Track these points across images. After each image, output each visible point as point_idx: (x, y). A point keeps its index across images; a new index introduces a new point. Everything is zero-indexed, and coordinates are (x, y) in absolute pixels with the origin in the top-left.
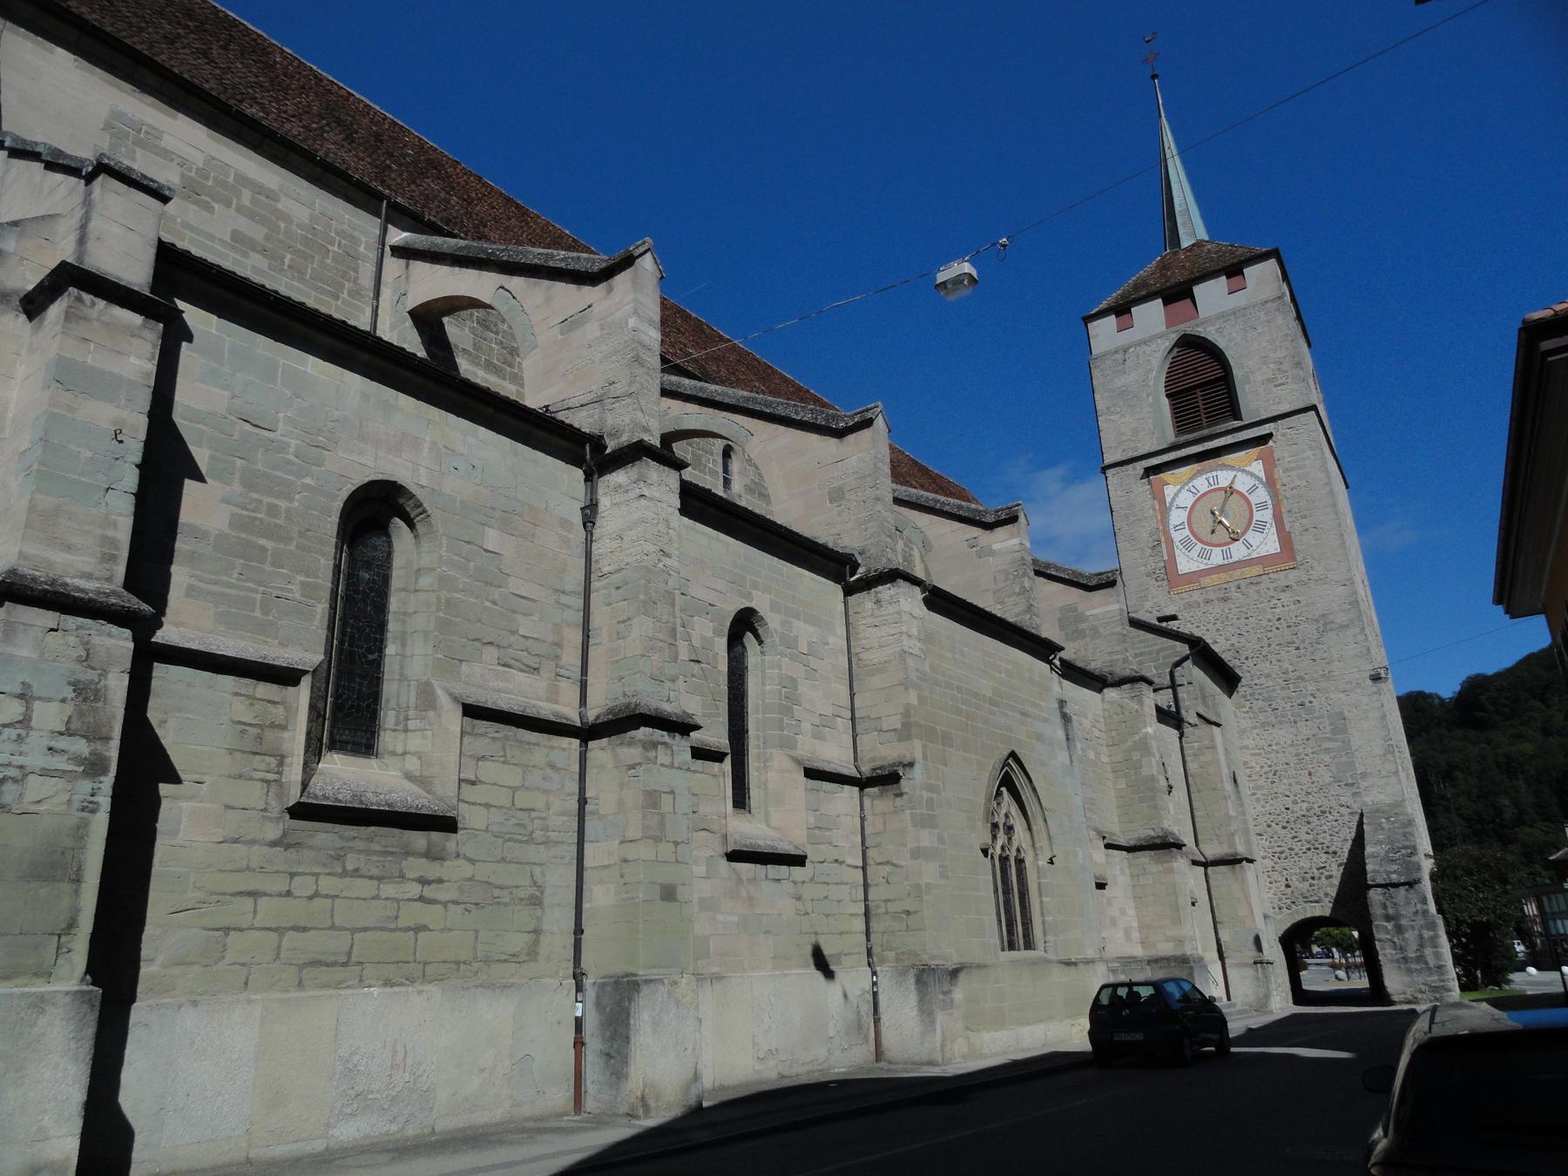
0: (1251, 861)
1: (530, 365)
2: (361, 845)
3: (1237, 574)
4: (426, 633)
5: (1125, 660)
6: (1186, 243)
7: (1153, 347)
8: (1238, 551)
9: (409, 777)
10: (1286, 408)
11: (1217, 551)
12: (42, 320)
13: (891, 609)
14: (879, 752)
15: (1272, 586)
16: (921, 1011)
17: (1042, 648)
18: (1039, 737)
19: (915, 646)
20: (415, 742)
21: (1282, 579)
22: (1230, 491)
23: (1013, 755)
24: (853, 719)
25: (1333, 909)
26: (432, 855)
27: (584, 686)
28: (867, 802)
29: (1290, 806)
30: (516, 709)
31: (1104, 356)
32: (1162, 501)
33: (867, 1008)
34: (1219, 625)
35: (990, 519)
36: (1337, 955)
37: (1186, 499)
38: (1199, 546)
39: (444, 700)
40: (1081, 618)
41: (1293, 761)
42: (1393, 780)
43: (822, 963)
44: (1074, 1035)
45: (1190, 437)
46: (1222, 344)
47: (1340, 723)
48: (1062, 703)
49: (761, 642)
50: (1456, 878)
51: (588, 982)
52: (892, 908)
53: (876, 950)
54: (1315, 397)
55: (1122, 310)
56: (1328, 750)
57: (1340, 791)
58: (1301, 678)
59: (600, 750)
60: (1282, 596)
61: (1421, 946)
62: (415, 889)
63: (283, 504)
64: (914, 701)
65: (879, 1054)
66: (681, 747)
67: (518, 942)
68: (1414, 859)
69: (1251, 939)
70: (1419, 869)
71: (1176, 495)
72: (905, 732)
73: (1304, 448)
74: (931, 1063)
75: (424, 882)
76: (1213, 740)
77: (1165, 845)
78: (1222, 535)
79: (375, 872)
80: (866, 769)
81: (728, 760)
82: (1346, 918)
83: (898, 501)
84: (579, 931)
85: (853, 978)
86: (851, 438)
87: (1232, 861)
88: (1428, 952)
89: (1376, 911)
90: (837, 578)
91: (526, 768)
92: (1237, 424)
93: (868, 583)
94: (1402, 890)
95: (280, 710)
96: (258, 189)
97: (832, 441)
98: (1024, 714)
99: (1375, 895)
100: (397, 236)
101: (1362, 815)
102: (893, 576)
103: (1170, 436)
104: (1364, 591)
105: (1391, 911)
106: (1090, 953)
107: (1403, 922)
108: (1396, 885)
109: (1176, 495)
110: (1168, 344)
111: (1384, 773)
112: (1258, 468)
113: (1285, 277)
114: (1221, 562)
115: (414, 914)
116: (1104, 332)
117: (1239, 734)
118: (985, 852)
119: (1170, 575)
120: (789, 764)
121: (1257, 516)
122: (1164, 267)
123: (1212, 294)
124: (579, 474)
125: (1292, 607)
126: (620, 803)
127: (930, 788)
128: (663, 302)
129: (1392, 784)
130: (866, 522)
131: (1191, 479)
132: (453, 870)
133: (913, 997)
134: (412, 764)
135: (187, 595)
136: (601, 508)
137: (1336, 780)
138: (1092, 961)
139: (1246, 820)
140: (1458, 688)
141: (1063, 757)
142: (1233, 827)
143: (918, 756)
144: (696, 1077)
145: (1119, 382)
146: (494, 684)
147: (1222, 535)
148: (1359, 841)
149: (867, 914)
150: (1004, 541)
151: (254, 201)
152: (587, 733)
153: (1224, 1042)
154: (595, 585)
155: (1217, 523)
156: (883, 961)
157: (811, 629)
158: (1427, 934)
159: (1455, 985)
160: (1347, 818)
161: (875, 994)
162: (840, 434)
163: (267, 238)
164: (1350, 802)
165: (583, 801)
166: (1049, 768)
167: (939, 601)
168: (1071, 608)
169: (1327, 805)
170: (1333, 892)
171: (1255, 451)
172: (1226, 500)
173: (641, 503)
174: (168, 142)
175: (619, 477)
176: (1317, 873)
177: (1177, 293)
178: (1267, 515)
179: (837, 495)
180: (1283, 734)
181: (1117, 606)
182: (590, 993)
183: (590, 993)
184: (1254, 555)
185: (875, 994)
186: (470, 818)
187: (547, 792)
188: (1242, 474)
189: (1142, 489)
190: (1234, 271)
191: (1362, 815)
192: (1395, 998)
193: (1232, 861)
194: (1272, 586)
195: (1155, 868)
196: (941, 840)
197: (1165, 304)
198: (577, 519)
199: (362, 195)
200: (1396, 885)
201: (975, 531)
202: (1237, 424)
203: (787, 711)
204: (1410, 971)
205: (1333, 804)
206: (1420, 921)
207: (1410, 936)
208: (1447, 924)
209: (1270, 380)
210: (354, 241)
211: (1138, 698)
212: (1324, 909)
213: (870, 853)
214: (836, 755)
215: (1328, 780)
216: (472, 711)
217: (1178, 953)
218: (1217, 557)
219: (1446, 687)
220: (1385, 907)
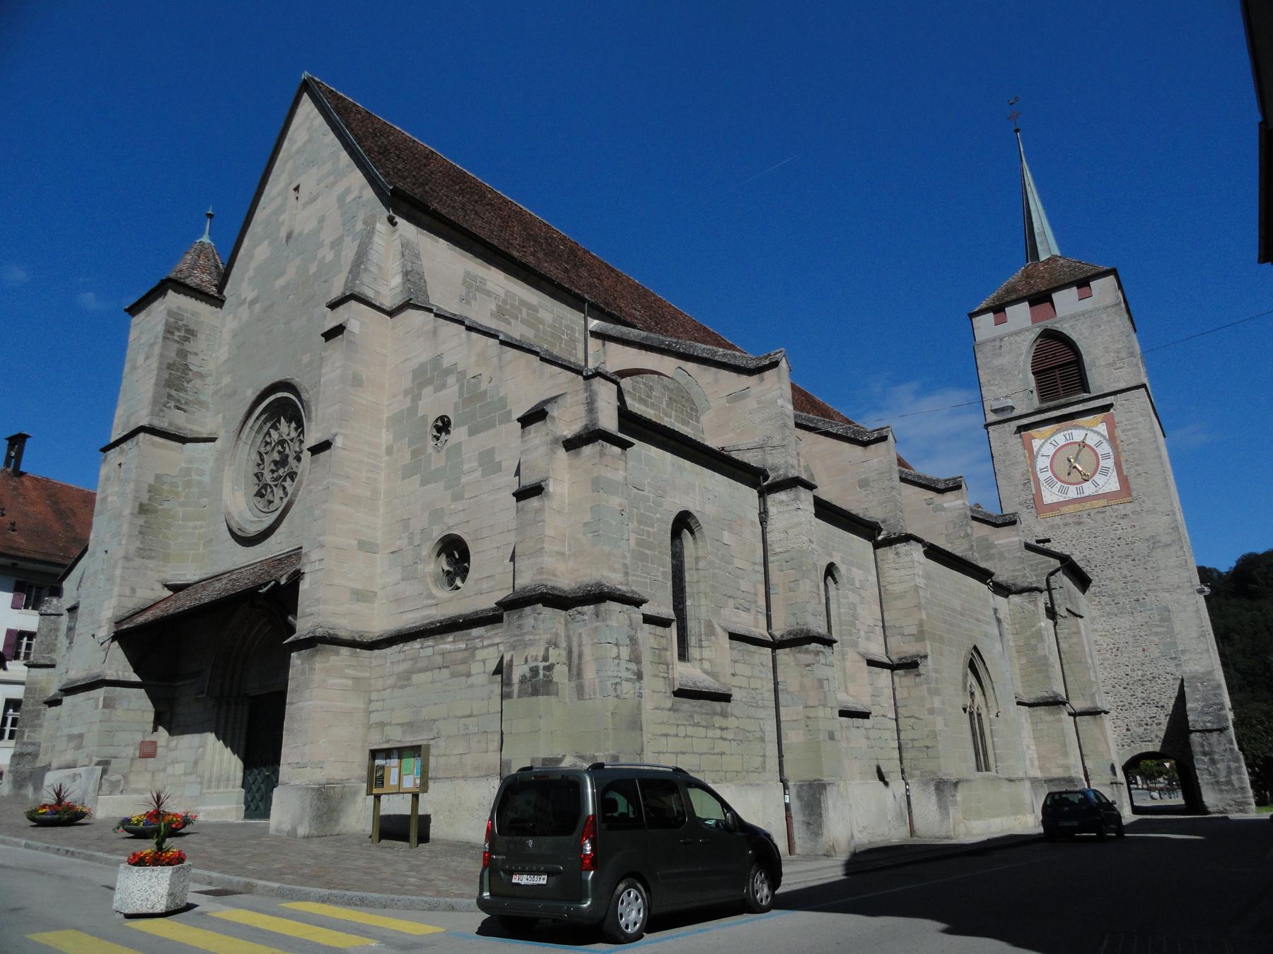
0: (1106, 713)
1: (706, 418)
2: (697, 709)
3: (1088, 505)
4: (706, 594)
5: (1024, 576)
6: (1043, 257)
7: (1022, 337)
8: (1089, 489)
9: (705, 672)
10: (1123, 386)
11: (1073, 488)
12: (578, 454)
14: (903, 648)
16: (940, 807)
17: (982, 575)
18: (986, 634)
19: (920, 581)
20: (707, 653)
21: (1122, 509)
22: (1083, 445)
23: (975, 648)
24: (884, 627)
25: (1162, 746)
26: (724, 715)
27: (769, 617)
28: (896, 679)
30: (746, 633)
31: (984, 343)
32: (1031, 451)
33: (904, 805)
35: (941, 486)
36: (1140, 782)
37: (1049, 450)
38: (1059, 484)
39: (719, 630)
40: (991, 546)
41: (1131, 640)
42: (1205, 655)
43: (881, 777)
44: (1029, 822)
46: (1074, 336)
47: (1166, 616)
48: (995, 610)
49: (836, 582)
50: (1253, 726)
51: (790, 784)
52: (916, 744)
53: (907, 770)
54: (1145, 380)
55: (998, 309)
56: (1157, 634)
57: (1165, 663)
58: (1135, 581)
59: (783, 654)
60: (1122, 521)
61: (1229, 772)
62: (718, 733)
63: (651, 529)
64: (924, 617)
65: (912, 832)
66: (636, 614)
67: (757, 761)
68: (1223, 712)
69: (1109, 768)
70: (1227, 719)
72: (920, 636)
73: (1135, 413)
74: (947, 838)
75: (722, 729)
76: (1078, 627)
77: (1054, 703)
78: (1076, 476)
79: (704, 724)
80: (895, 658)
81: (674, 625)
82: (1174, 755)
83: (798, 425)
84: (781, 756)
85: (897, 786)
86: (873, 447)
87: (1094, 713)
88: (1234, 777)
89: (1196, 748)
90: (754, 485)
91: (752, 665)
92: (1086, 395)
93: (889, 542)
94: (1215, 734)
95: (664, 641)
96: (531, 307)
97: (860, 448)
98: (977, 620)
99: (1195, 738)
100: (594, 324)
101: (1182, 680)
102: (908, 538)
103: (1036, 403)
104: (1180, 517)
106: (1021, 775)
107: (1216, 757)
108: (1210, 731)
110: (1033, 336)
112: (1102, 428)
113: (1120, 287)
115: (721, 746)
116: (985, 325)
117: (1096, 625)
118: (965, 710)
119: (1037, 503)
120: (858, 658)
121: (1102, 463)
122: (1028, 276)
123: (1066, 300)
124: (755, 492)
126: (802, 685)
127: (936, 671)
128: (793, 387)
129: (1203, 660)
131: (1052, 435)
132: (731, 722)
133: (934, 799)
134: (706, 665)
136: (770, 513)
138: (1021, 780)
139: (1098, 681)
140: (1234, 564)
141: (999, 646)
142: (1094, 690)
143: (929, 652)
144: (852, 837)
145: (997, 362)
146: (734, 619)
147: (1076, 476)
148: (1181, 698)
149: (900, 748)
150: (951, 501)
151: (528, 314)
152: (776, 645)
153: (1121, 829)
154: (771, 559)
155: (1073, 467)
156: (912, 776)
157: (860, 572)
158: (1233, 765)
159: (1252, 801)
161: (908, 797)
162: (865, 444)
163: (536, 336)
164: (1174, 670)
165: (776, 684)
166: (993, 653)
167: (934, 553)
168: (985, 539)
169: (1156, 672)
170: (1162, 735)
171: (1100, 416)
172: (1079, 451)
173: (791, 512)
174: (490, 286)
175: (782, 496)
176: (1150, 721)
177: (1040, 299)
178: (1110, 463)
179: (864, 484)
180: (1124, 622)
181: (1017, 539)
182: (793, 790)
183: (793, 790)
185: (908, 797)
186: (736, 695)
187: (761, 679)
188: (1091, 432)
189: (1015, 441)
190: (1083, 283)
191: (1182, 680)
192: (1211, 810)
193: (1094, 713)
195: (1049, 718)
196: (943, 703)
197: (1031, 305)
198: (757, 520)
199: (574, 300)
200: (1210, 731)
201: (931, 494)
202: (1086, 395)
203: (853, 624)
204: (1221, 791)
205: (1161, 672)
206: (1228, 755)
207: (1221, 766)
208: (1246, 758)
210: (573, 330)
211: (1035, 602)
212: (1155, 747)
213: (900, 710)
214: (878, 652)
215: (1157, 655)
216: (733, 636)
217: (1066, 775)
218: (1072, 493)
219: (1225, 563)
220: (1202, 746)
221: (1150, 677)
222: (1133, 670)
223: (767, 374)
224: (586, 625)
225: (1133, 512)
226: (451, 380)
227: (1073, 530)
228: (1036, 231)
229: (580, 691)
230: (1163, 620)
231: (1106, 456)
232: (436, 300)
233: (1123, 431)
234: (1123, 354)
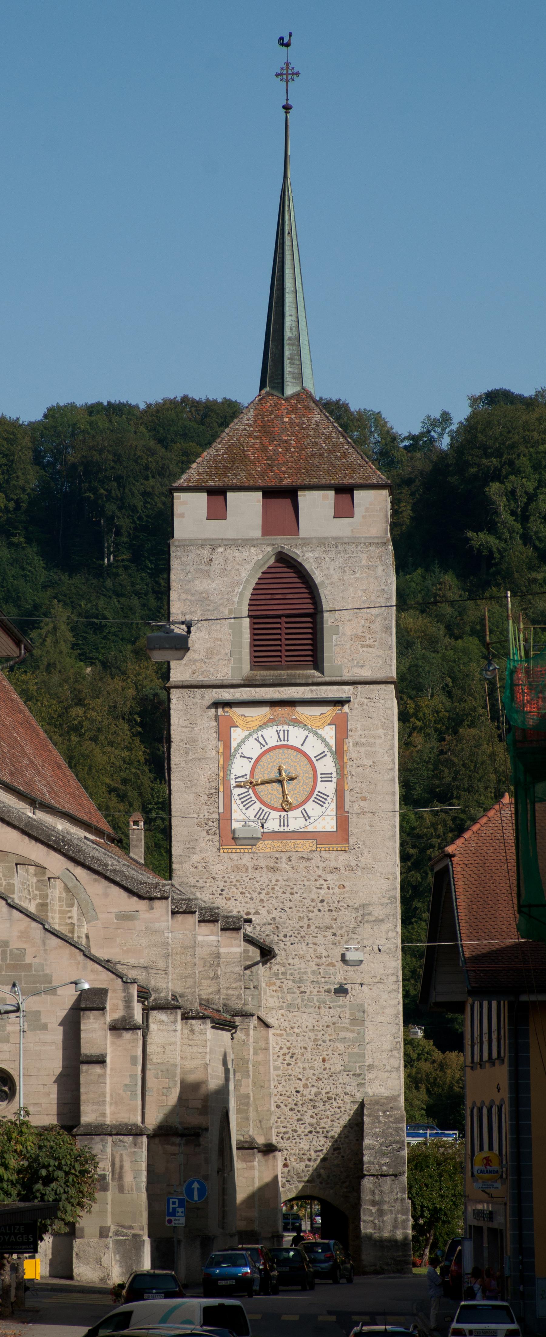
5: (239, 997)
6: (290, 390)
8: (296, 822)
10: (366, 674)
13: (200, 1037)
15: (322, 865)
29: (301, 1089)
31: (189, 544)
34: (263, 896)
38: (258, 805)
41: (310, 1045)
46: (318, 577)
57: (347, 1080)
60: (329, 877)
71: (243, 741)
89: (366, 1196)
99: (367, 1183)
101: (362, 1105)
105: (377, 1197)
107: (385, 1207)
109: (243, 741)
111: (388, 1068)
112: (329, 733)
114: (277, 828)
121: (320, 787)
125: (337, 890)
129: (387, 1081)
130: (186, 977)
131: (261, 727)
137: (346, 1070)
145: (201, 585)
158: (401, 1217)
160: (348, 1106)
171: (328, 710)
178: (329, 788)
184: (310, 829)
188: (311, 736)
191: (362, 1105)
194: (322, 865)
205: (340, 1091)
206: (398, 1206)
209: (358, 638)
220: (373, 1193)
221: (324, 1096)
222: (306, 1086)
224: (127, 1149)
225: (347, 867)
227: (264, 877)
228: (288, 334)
229: (121, 1188)
230: (354, 1021)
231: (327, 777)
233: (356, 744)
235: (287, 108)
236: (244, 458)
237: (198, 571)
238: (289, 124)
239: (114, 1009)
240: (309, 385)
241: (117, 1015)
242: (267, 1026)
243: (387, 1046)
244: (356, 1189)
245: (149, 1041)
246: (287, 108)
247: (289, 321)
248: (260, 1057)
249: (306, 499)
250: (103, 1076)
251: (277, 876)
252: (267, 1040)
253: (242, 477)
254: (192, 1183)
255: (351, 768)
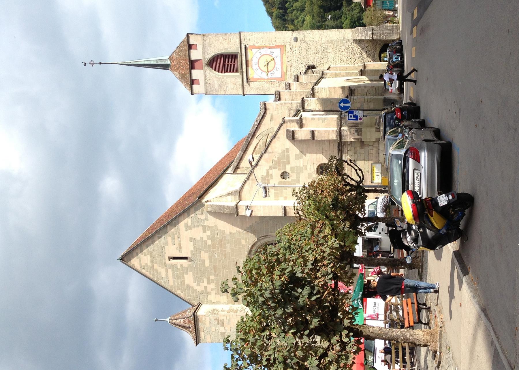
3: (284, 61)
6: (169, 62)
8: (278, 60)
10: (238, 40)
11: (277, 66)
38: (274, 70)
41: (338, 55)
45: (239, 70)
47: (331, 42)
89: (378, 38)
99: (375, 38)
101: (354, 40)
103: (238, 74)
108: (373, 33)
112: (254, 50)
129: (348, 34)
135: (190, 238)
137: (344, 45)
145: (216, 86)
158: (384, 27)
171: (249, 51)
177: (192, 64)
178: (269, 50)
182: (385, 107)
189: (252, 84)
223: (267, 107)
226: (271, 172)
228: (155, 63)
230: (331, 43)
231: (266, 51)
232: (238, 187)
234: (225, 37)
235: (100, 63)
236: (184, 75)
237: (213, 87)
238: (121, 62)
239: (294, 127)
240: (168, 57)
241: (296, 125)
242: (329, 67)
243: (338, 33)
244: (376, 40)
245: (314, 109)
246: (100, 63)
247: (152, 63)
248: (338, 69)
249: (193, 58)
250: (318, 131)
251: (293, 65)
252: (334, 67)
253: (188, 75)
254: (340, 107)
255: (263, 45)
